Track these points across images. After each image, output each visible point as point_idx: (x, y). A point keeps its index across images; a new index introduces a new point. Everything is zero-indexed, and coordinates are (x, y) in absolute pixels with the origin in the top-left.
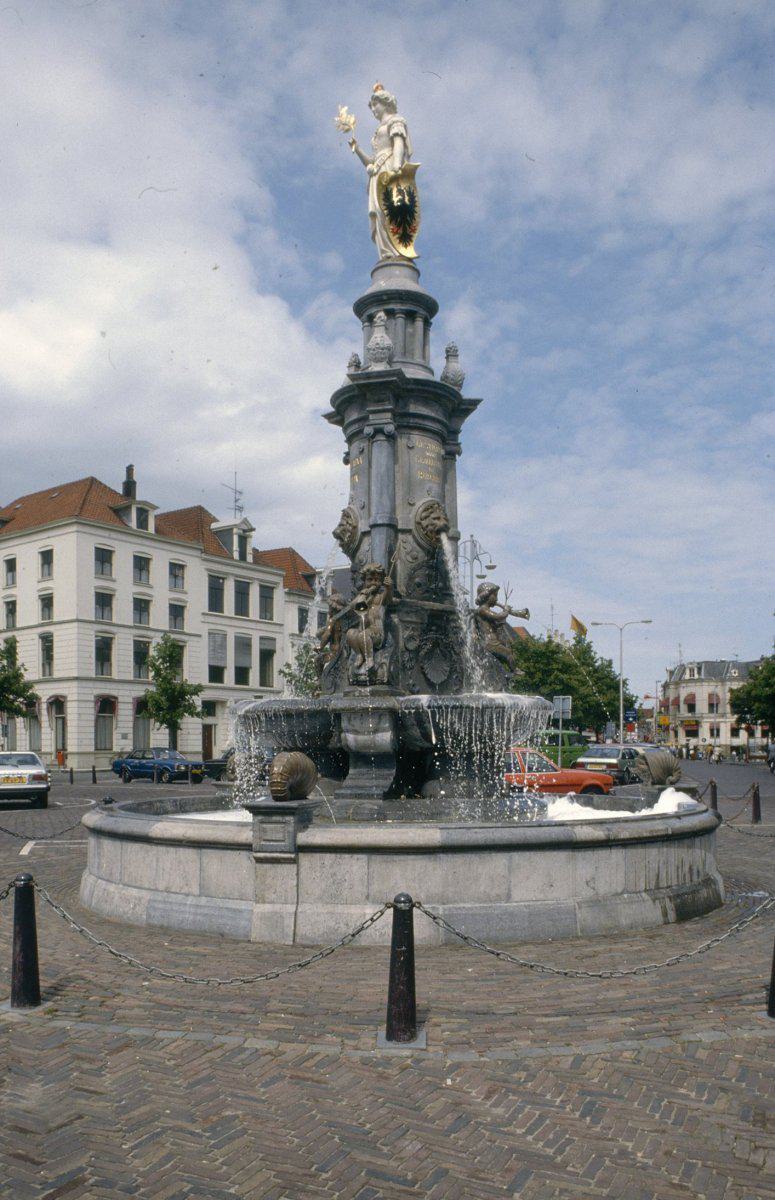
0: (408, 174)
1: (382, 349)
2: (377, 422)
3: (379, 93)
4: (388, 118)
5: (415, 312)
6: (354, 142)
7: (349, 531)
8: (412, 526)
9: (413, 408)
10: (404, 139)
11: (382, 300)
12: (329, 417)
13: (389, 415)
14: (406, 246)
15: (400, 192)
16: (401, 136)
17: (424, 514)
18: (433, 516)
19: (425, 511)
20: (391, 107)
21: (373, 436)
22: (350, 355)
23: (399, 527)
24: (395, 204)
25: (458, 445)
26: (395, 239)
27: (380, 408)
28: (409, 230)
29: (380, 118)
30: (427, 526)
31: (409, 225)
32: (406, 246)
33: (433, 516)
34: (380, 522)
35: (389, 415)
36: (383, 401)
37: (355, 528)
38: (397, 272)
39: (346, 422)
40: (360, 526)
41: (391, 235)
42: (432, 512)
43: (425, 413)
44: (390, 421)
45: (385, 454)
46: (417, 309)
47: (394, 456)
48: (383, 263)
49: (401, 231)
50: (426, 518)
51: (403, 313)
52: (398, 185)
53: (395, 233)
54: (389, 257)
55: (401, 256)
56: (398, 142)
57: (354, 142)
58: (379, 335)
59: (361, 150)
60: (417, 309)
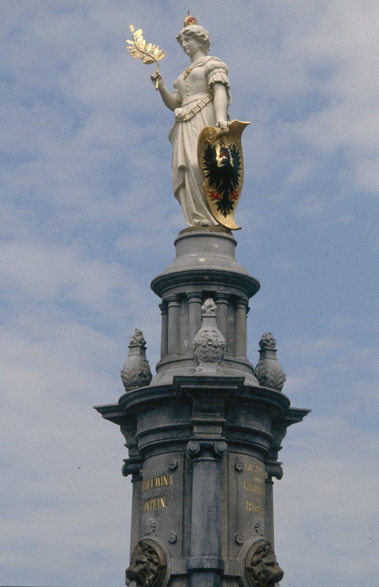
0: (236, 130)
1: (215, 347)
2: (204, 436)
3: (193, 28)
4: (201, 58)
5: (239, 298)
6: (158, 77)
7: (152, 571)
8: (240, 573)
9: (242, 423)
10: (225, 85)
11: (203, 280)
12: (105, 411)
13: (219, 430)
14: (225, 214)
15: (224, 152)
16: (225, 85)
17: (255, 558)
18: (265, 560)
19: (256, 553)
20: (204, 44)
21: (199, 454)
22: (134, 333)
23: (225, 573)
24: (219, 165)
25: (279, 465)
26: (213, 204)
27: (210, 420)
28: (230, 196)
29: (192, 56)
30: (259, 574)
31: (232, 190)
32: (225, 214)
33: (265, 560)
34: (207, 565)
35: (219, 430)
36: (214, 411)
37: (163, 568)
38: (216, 246)
39: (140, 430)
40: (169, 566)
41: (209, 199)
42: (264, 556)
43: (257, 429)
44: (219, 437)
45: (212, 478)
46: (236, 290)
47: (222, 481)
48: (194, 233)
49: (221, 196)
50: (258, 562)
51: (225, 299)
52: (222, 143)
53: (214, 197)
54: (205, 226)
55: (220, 225)
56: (220, 93)
57: (158, 77)
58: (210, 328)
59: (165, 87)
60: (236, 290)
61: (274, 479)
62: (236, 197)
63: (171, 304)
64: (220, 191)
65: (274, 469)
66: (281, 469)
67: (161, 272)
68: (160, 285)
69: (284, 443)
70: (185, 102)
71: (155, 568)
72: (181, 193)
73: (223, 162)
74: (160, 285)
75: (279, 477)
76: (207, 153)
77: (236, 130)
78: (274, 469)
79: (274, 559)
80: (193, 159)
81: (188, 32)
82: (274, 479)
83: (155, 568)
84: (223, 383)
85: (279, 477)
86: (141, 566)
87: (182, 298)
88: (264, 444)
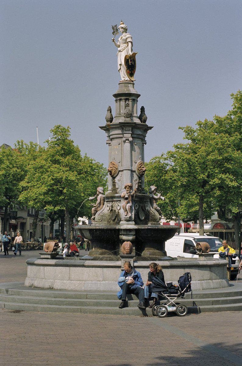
0: (134, 55)
14: (131, 77)
22: (108, 107)
32: (131, 77)
48: (123, 82)
49: (130, 72)
50: (140, 167)
61: (144, 144)
62: (134, 72)
63: (118, 101)
64: (130, 71)
65: (144, 142)
66: (146, 142)
67: (114, 94)
68: (116, 96)
69: (147, 135)
70: (121, 46)
71: (115, 169)
72: (120, 70)
73: (131, 63)
74: (116, 96)
75: (146, 144)
76: (127, 61)
77: (134, 55)
78: (144, 142)
79: (157, 248)
80: (123, 63)
81: (220, 346)
82: (144, 144)
83: (115, 169)
84: (132, 124)
85: (146, 144)
86: (111, 168)
87: (120, 100)
88: (142, 137)
